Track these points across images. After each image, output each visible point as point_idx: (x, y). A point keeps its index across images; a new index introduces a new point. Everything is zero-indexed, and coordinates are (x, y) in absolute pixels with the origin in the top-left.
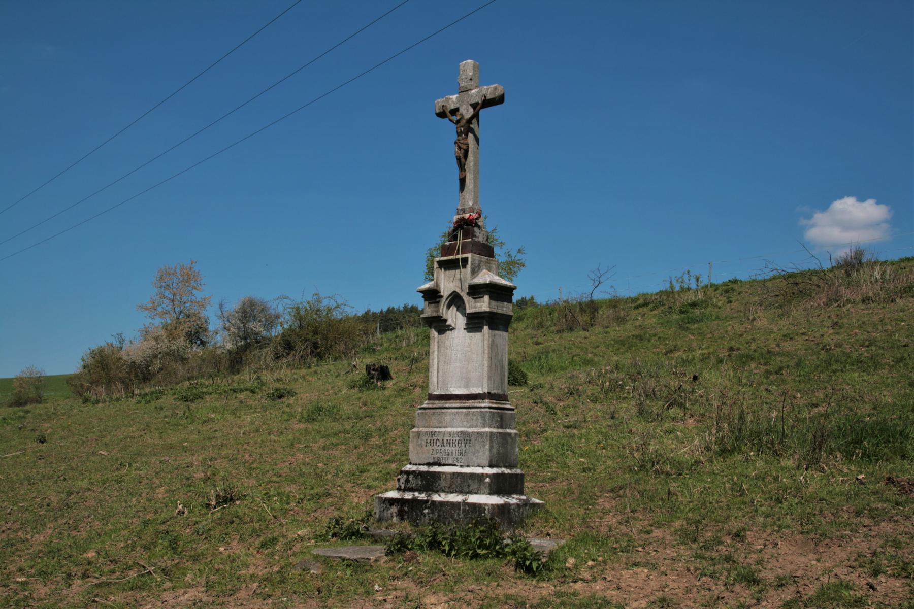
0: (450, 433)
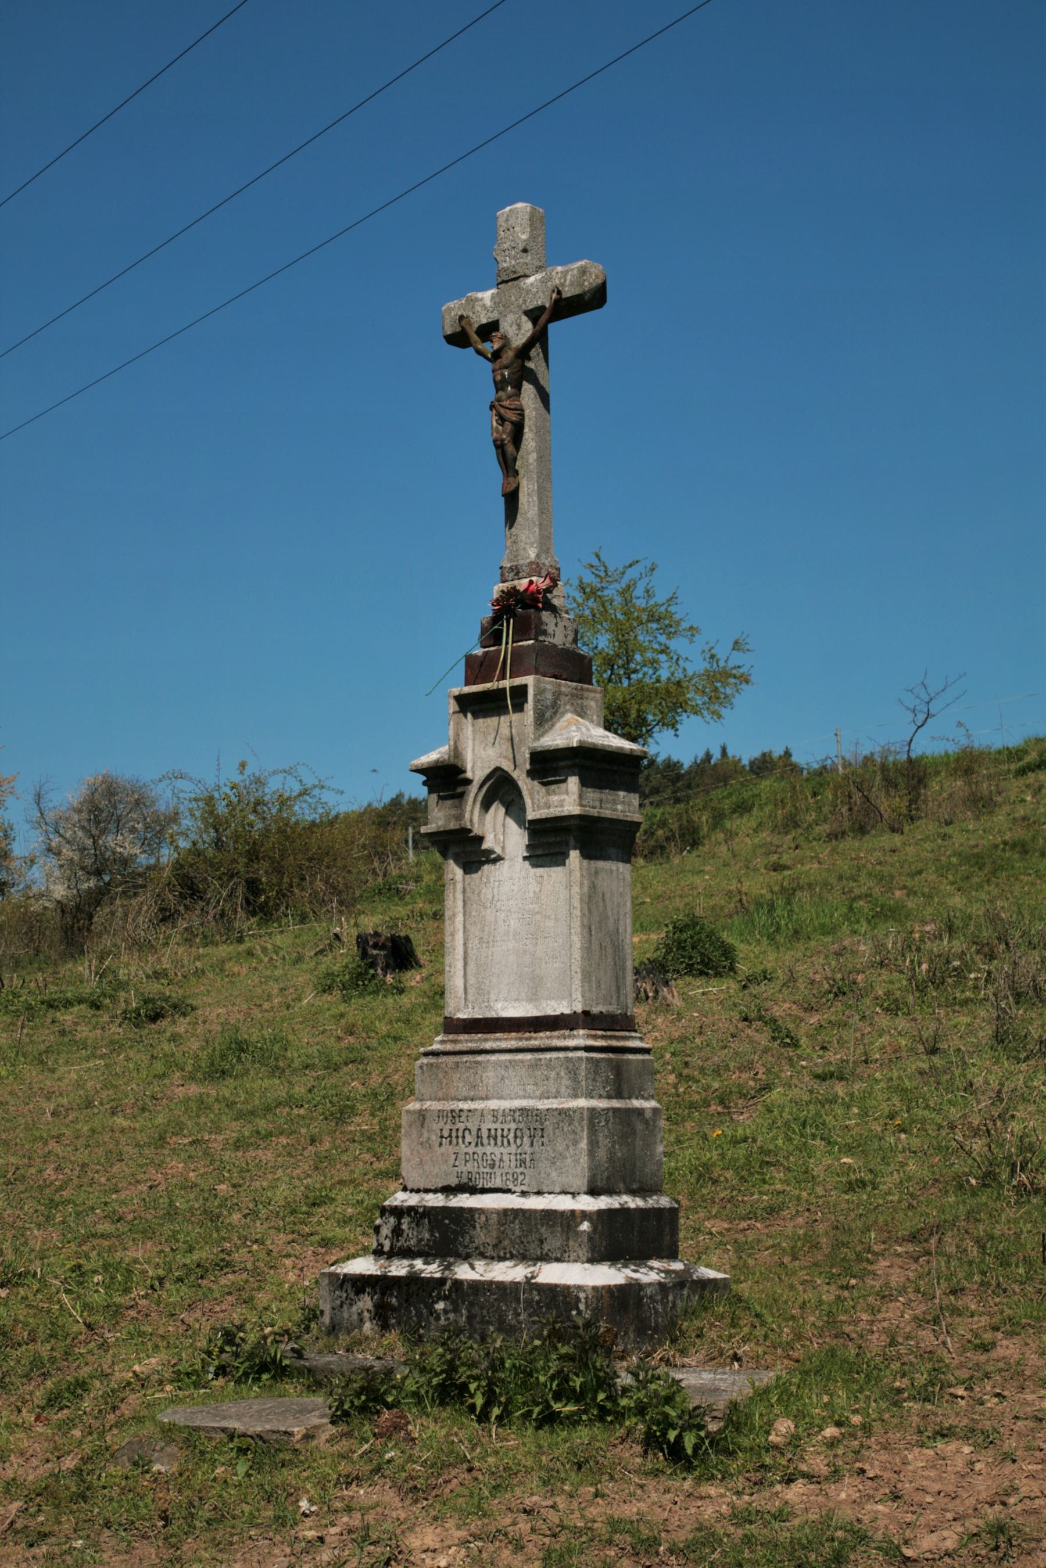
0: (494, 1113)
